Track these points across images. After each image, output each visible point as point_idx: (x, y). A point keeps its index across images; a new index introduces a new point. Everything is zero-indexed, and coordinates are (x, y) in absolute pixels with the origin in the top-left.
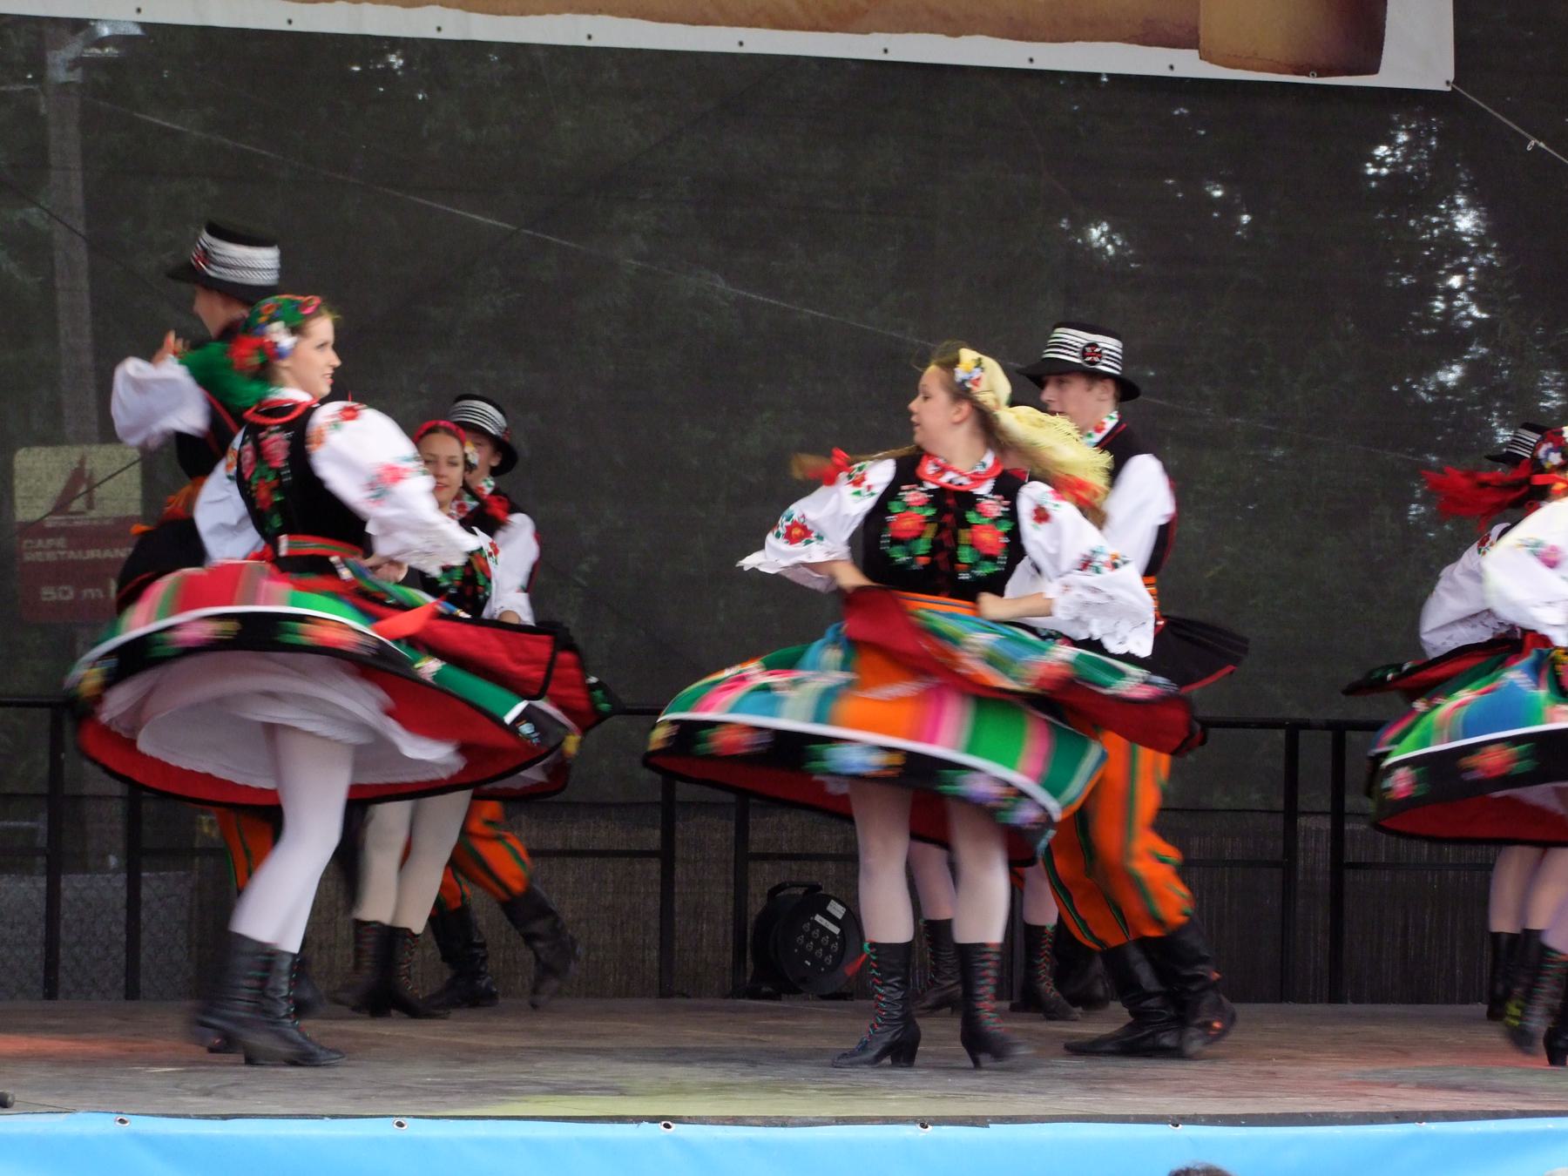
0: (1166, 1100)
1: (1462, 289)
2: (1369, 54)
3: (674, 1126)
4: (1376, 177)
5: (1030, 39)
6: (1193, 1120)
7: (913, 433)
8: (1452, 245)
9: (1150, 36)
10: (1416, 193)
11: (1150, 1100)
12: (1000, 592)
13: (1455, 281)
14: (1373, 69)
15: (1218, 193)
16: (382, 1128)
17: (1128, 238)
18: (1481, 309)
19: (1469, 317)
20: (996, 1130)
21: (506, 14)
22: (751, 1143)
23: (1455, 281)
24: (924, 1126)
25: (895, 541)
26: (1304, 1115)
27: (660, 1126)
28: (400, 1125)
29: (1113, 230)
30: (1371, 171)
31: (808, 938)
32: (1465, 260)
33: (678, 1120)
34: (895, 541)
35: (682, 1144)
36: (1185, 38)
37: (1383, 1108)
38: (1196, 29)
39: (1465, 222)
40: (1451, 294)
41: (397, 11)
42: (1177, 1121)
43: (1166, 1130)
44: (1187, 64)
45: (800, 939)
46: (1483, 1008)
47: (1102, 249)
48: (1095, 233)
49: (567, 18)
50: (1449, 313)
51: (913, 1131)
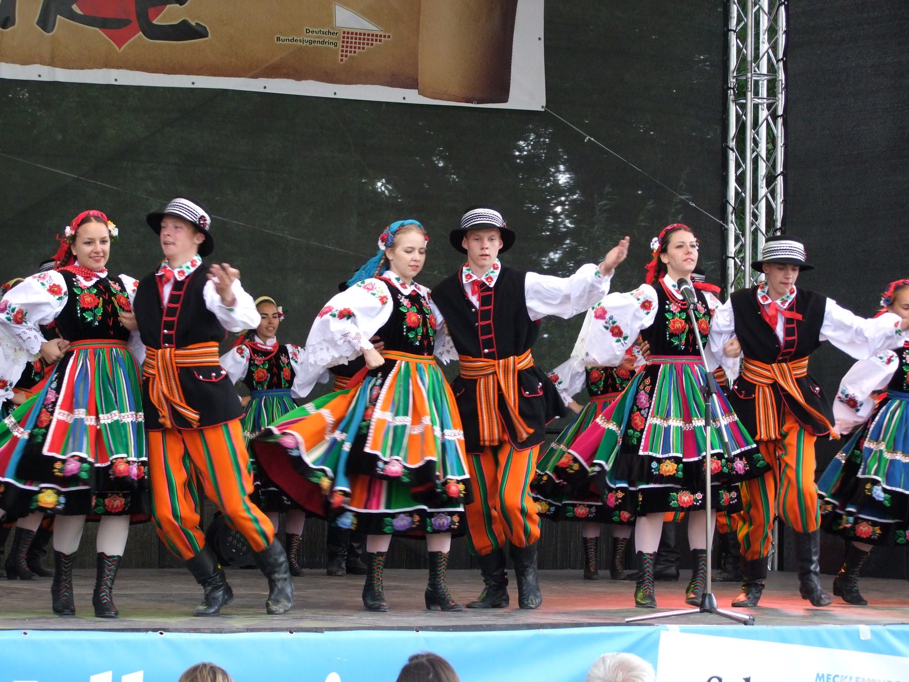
0: (413, 619)
1: (561, 213)
2: (503, 93)
3: (165, 633)
4: (520, 157)
5: (335, 82)
6: (426, 628)
7: (140, 283)
8: (558, 190)
9: (395, 81)
10: (538, 167)
11: (405, 619)
12: (848, 362)
13: (559, 209)
14: (505, 100)
15: (441, 165)
16: (17, 635)
17: (395, 186)
18: (571, 223)
19: (566, 227)
20: (328, 634)
21: (73, 68)
22: (205, 642)
23: (559, 209)
24: (291, 632)
25: (672, 335)
26: (481, 626)
27: (158, 634)
28: (25, 634)
29: (388, 182)
30: (517, 153)
31: (234, 537)
32: (563, 199)
33: (167, 630)
34: (672, 335)
35: (169, 643)
36: (411, 83)
37: (521, 622)
38: (417, 80)
39: (563, 179)
40: (556, 216)
41: (18, 67)
42: (418, 629)
43: (413, 634)
44: (412, 97)
45: (230, 539)
46: (582, 572)
47: (383, 192)
48: (379, 184)
49: (104, 71)
50: (556, 224)
51: (286, 635)
